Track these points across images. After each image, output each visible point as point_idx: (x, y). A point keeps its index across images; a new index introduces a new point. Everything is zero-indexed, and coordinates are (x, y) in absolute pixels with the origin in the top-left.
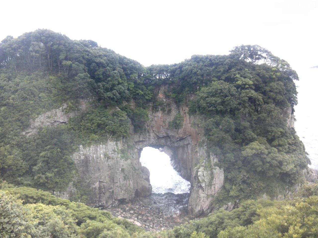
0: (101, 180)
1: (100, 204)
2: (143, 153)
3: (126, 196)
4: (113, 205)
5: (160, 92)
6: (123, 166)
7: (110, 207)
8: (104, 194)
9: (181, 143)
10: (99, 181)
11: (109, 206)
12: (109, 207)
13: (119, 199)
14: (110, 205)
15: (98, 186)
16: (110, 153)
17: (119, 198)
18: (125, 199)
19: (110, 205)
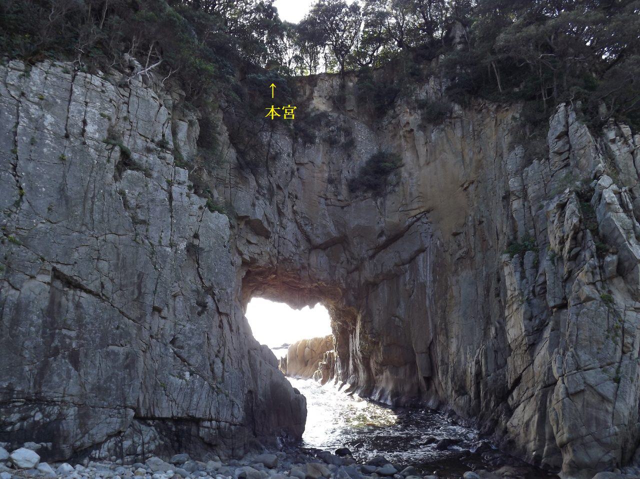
0: (66, 270)
1: (39, 417)
2: (250, 306)
3: (202, 404)
4: (127, 444)
5: (316, 94)
6: (196, 236)
7: (103, 452)
8: (74, 359)
9: (389, 259)
10: (57, 275)
11: (97, 446)
12: (96, 453)
13: (166, 414)
14: (109, 437)
15: (45, 304)
16: (140, 142)
17: (165, 410)
18: (197, 421)
19: (109, 437)
